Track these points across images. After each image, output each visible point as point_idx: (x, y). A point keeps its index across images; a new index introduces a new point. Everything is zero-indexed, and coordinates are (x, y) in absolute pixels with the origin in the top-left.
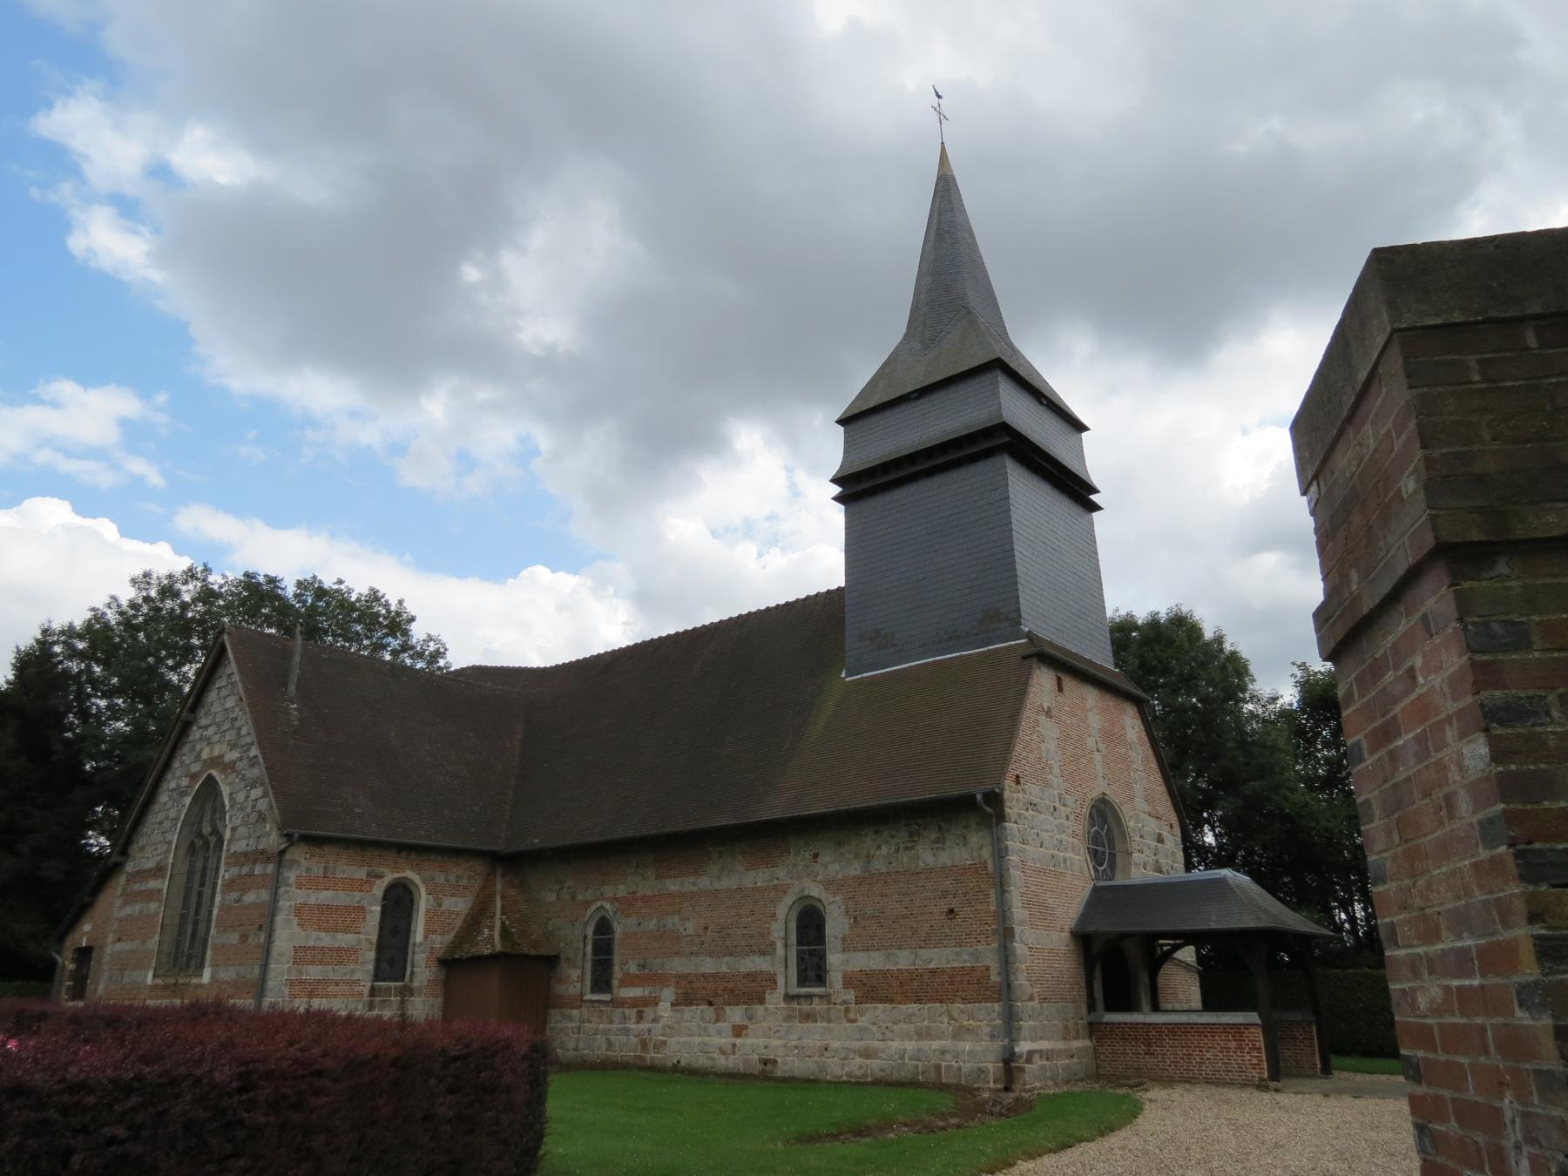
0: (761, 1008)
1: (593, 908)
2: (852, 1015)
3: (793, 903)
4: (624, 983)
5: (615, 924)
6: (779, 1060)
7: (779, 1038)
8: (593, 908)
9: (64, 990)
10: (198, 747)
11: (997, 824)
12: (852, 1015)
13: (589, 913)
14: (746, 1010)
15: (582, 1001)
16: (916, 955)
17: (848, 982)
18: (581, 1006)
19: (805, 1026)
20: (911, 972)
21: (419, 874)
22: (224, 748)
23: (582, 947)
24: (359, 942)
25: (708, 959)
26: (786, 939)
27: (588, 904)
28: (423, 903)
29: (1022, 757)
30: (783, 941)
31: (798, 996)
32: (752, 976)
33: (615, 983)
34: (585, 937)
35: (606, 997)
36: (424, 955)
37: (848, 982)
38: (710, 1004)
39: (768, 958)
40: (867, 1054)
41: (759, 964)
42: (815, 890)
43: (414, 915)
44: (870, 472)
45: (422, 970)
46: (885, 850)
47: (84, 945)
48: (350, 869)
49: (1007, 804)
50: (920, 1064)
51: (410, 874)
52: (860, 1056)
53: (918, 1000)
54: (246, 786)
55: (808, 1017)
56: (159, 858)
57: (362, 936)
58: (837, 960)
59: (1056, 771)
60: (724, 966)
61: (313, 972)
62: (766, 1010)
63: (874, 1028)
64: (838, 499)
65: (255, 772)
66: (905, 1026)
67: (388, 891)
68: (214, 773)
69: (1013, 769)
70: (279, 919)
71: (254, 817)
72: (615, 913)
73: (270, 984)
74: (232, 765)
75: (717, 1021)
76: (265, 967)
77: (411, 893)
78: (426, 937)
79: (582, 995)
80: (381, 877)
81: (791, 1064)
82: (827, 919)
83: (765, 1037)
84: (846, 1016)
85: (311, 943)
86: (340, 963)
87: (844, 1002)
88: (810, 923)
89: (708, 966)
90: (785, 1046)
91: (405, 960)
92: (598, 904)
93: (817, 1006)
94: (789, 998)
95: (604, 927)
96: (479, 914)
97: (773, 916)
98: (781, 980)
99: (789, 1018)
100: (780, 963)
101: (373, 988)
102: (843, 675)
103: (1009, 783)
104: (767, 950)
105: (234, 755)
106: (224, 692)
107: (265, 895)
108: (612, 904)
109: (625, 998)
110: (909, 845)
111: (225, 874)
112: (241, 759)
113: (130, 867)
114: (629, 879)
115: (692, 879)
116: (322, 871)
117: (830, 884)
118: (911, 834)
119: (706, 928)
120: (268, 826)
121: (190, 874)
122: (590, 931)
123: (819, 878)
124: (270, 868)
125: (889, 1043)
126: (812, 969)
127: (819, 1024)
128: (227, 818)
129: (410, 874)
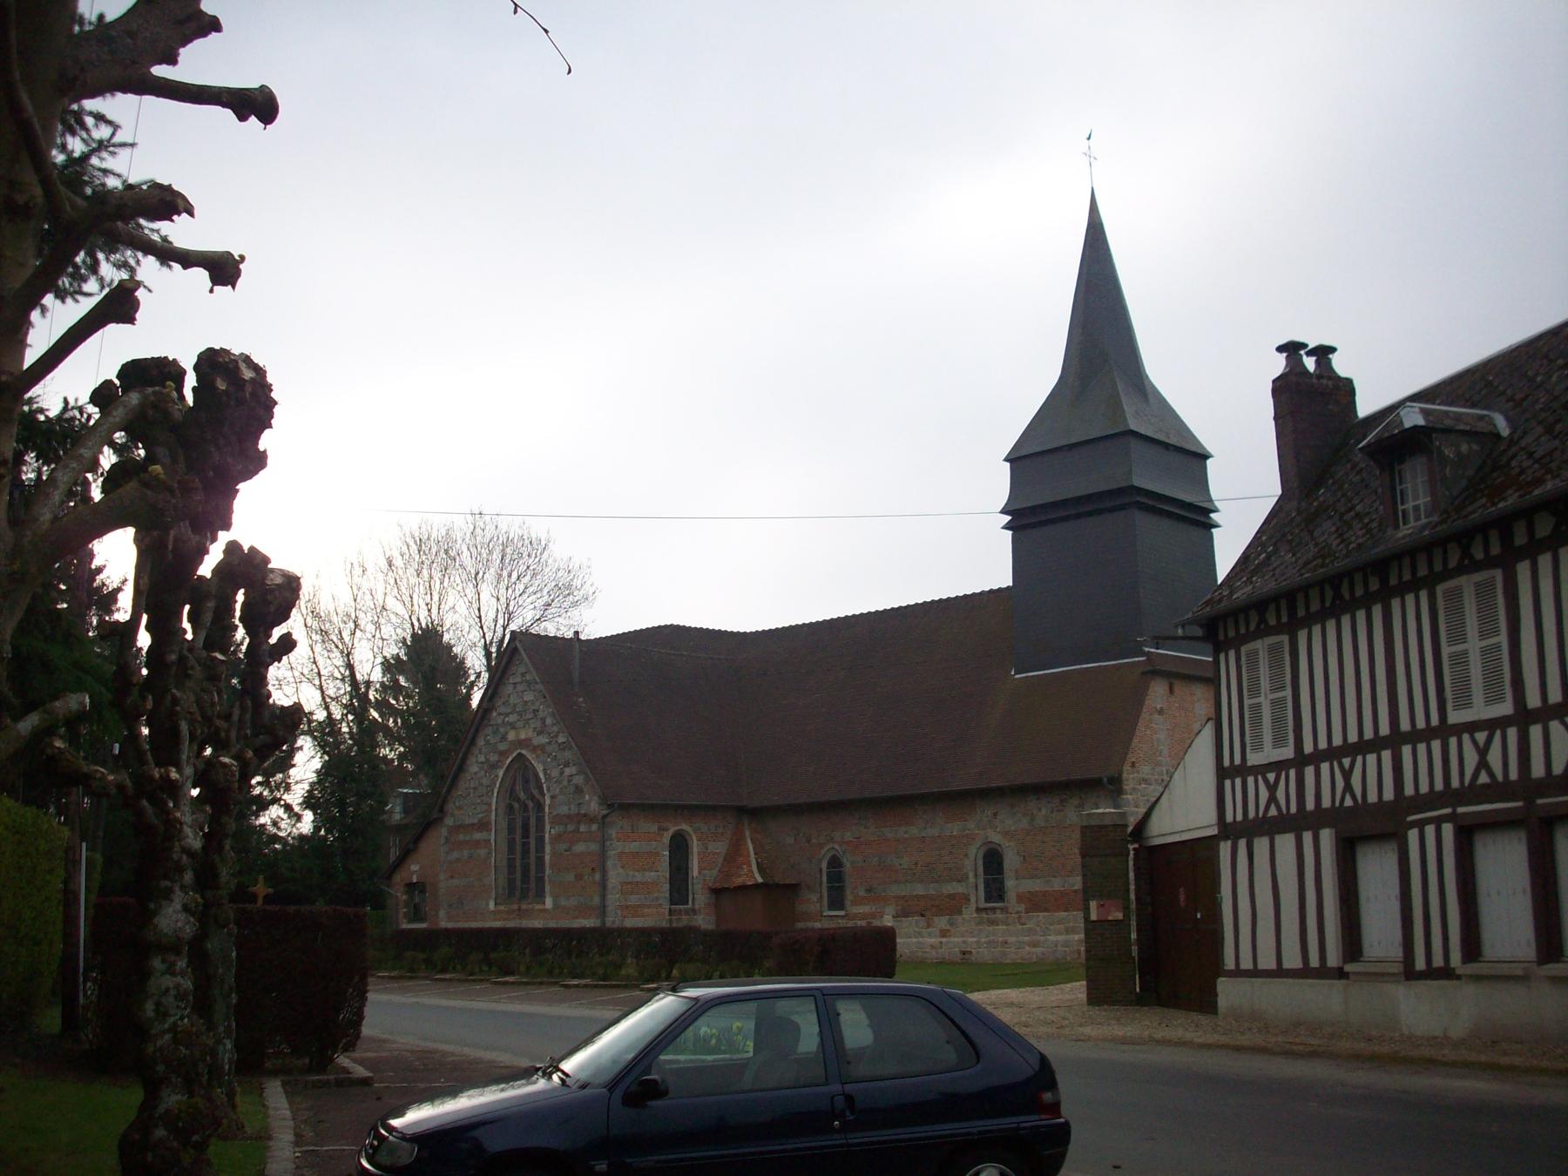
0: (959, 918)
1: (826, 849)
2: (1023, 921)
3: (981, 846)
4: (854, 903)
5: (845, 861)
6: (973, 951)
7: (973, 937)
8: (826, 849)
9: (401, 915)
10: (502, 730)
11: (1118, 796)
12: (1023, 921)
13: (823, 852)
14: (949, 920)
15: (822, 916)
16: (1065, 881)
17: (1020, 898)
18: (821, 920)
19: (991, 928)
20: (1061, 892)
21: (691, 826)
22: (530, 734)
23: (819, 877)
24: (658, 876)
25: (919, 885)
26: (976, 871)
27: (821, 846)
28: (695, 847)
29: (1138, 748)
30: (973, 873)
31: (986, 909)
32: (952, 897)
33: (848, 903)
34: (821, 870)
35: (842, 913)
36: (700, 886)
37: (1020, 898)
38: (923, 916)
39: (964, 884)
40: (1035, 944)
41: (958, 888)
42: (996, 838)
43: (690, 857)
44: (1034, 510)
45: (699, 897)
46: (1044, 811)
47: (415, 881)
48: (648, 826)
49: (1125, 782)
50: (1067, 949)
51: (685, 827)
52: (1029, 945)
53: (1066, 910)
54: (559, 765)
55: (993, 922)
56: (481, 815)
57: (659, 873)
58: (1010, 883)
59: (1166, 752)
60: (932, 890)
61: (634, 900)
62: (964, 919)
63: (1038, 929)
64: (1006, 527)
65: (568, 754)
66: (1059, 926)
67: (673, 837)
68: (524, 752)
69: (1131, 758)
70: (609, 863)
71: (572, 789)
72: (844, 852)
73: (609, 909)
74: (542, 747)
75: (928, 926)
76: (603, 897)
77: (686, 840)
78: (699, 873)
79: (821, 912)
80: (667, 830)
81: (985, 954)
82: (1005, 857)
83: (963, 936)
84: (1019, 922)
85: (630, 880)
86: (649, 893)
87: (1018, 912)
88: (993, 861)
89: (919, 890)
90: (978, 942)
91: (687, 890)
92: (831, 846)
93: (999, 915)
94: (979, 910)
95: (835, 863)
96: (734, 856)
97: (966, 855)
98: (973, 899)
99: (979, 924)
100: (973, 885)
101: (670, 909)
102: (1013, 673)
103: (1127, 767)
104: (963, 879)
105: (543, 740)
106: (520, 688)
107: (594, 847)
108: (840, 846)
109: (856, 914)
110: (1061, 808)
111: (549, 831)
112: (550, 743)
113: (449, 821)
114: (854, 828)
115: (903, 828)
116: (630, 828)
117: (1006, 834)
118: (1062, 801)
119: (916, 864)
120: (587, 797)
121: (511, 830)
122: (824, 865)
123: (998, 830)
124: (594, 827)
125: (1048, 937)
126: (995, 891)
127: (1000, 927)
128: (545, 788)
129: (685, 827)
